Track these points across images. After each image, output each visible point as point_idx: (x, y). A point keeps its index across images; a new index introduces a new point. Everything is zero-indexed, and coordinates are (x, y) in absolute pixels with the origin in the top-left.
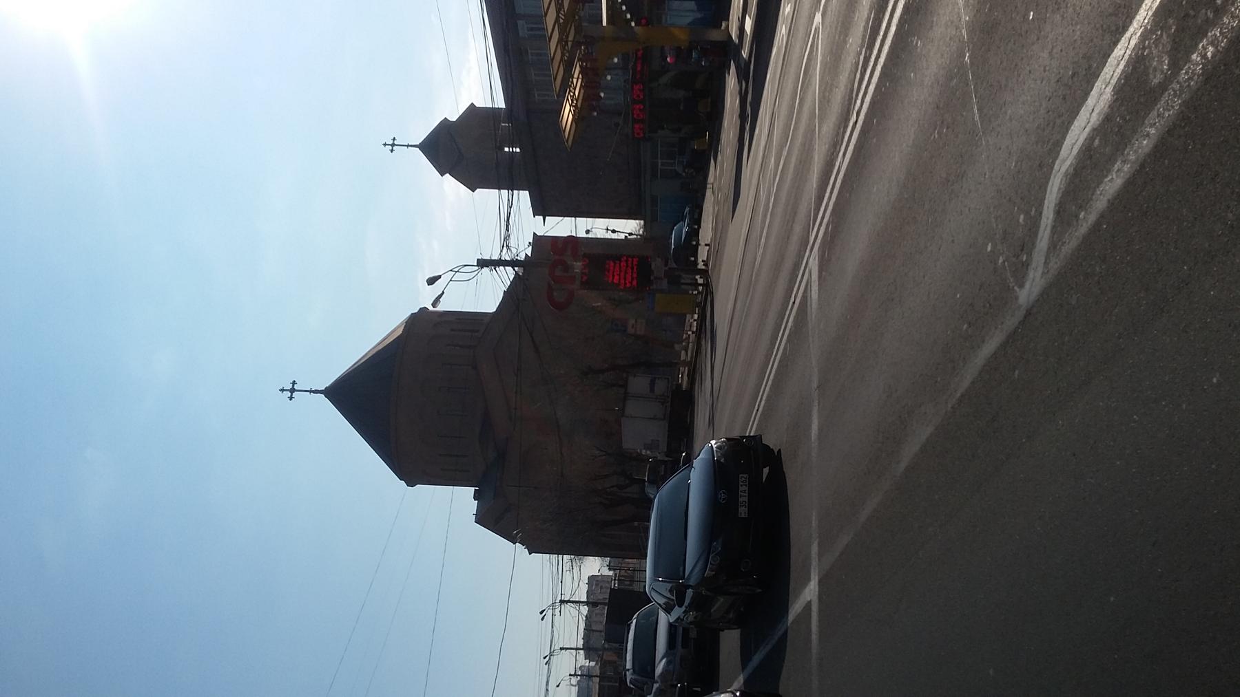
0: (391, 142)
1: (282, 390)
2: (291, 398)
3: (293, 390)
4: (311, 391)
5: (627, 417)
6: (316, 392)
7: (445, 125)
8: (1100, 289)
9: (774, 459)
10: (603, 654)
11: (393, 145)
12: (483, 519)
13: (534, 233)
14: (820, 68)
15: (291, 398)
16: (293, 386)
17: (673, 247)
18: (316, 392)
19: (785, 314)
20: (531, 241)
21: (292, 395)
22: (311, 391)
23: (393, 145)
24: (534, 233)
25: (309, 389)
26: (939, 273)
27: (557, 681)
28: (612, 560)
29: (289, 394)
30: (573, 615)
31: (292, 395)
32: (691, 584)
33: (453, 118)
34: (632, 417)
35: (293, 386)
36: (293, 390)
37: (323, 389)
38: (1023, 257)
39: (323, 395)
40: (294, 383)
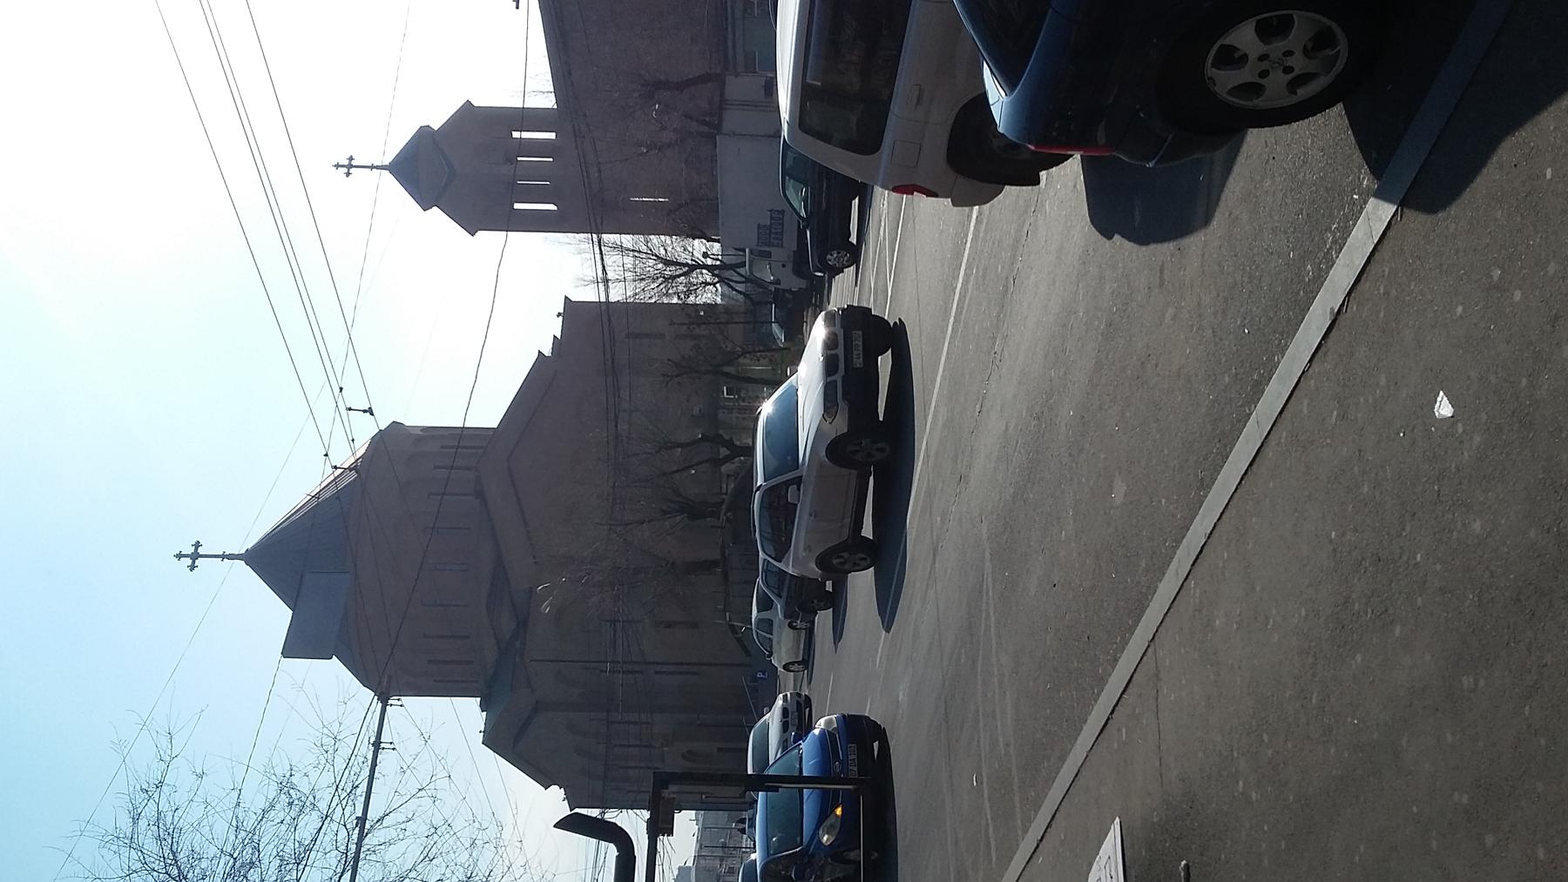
0: (346, 162)
1: (180, 556)
2: (192, 567)
3: (195, 556)
4: (224, 557)
5: (725, 134)
6: (231, 557)
7: (424, 134)
9: (878, 732)
10: (1053, 9)
11: (350, 166)
12: (493, 739)
13: (566, 297)
15: (192, 567)
16: (196, 549)
18: (231, 557)
20: (562, 311)
21: (194, 562)
22: (224, 557)
24: (566, 297)
25: (221, 553)
26: (1092, 405)
27: (1261, 437)
29: (189, 561)
31: (194, 562)
32: (830, 866)
33: (436, 126)
34: (734, 134)
35: (196, 549)
36: (195, 556)
38: (828, 839)
40: (197, 545)
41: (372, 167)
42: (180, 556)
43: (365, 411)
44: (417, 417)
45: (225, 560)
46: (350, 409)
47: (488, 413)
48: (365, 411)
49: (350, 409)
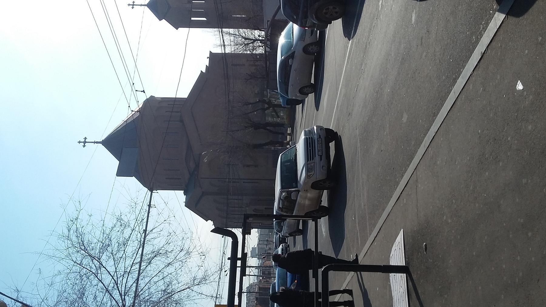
1: (80, 142)
2: (84, 146)
3: (85, 142)
4: (95, 142)
6: (97, 143)
8: (185, 271)
11: (133, 5)
12: (188, 205)
14: (277, 287)
15: (84, 146)
16: (85, 140)
17: (324, 267)
18: (97, 143)
19: (332, 120)
20: (209, 56)
21: (84, 144)
22: (95, 142)
23: (133, 5)
25: (94, 141)
28: (328, 190)
29: (83, 144)
30: (163, 237)
31: (84, 144)
35: (85, 140)
36: (85, 142)
37: (101, 141)
39: (101, 144)
41: (141, 5)
42: (80, 142)
43: (142, 91)
44: (159, 94)
45: (95, 143)
46: (137, 91)
47: (184, 93)
48: (142, 91)
49: (137, 91)
